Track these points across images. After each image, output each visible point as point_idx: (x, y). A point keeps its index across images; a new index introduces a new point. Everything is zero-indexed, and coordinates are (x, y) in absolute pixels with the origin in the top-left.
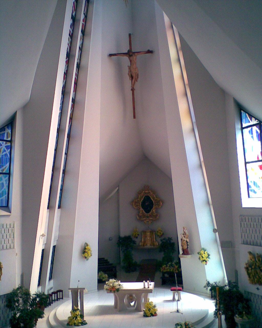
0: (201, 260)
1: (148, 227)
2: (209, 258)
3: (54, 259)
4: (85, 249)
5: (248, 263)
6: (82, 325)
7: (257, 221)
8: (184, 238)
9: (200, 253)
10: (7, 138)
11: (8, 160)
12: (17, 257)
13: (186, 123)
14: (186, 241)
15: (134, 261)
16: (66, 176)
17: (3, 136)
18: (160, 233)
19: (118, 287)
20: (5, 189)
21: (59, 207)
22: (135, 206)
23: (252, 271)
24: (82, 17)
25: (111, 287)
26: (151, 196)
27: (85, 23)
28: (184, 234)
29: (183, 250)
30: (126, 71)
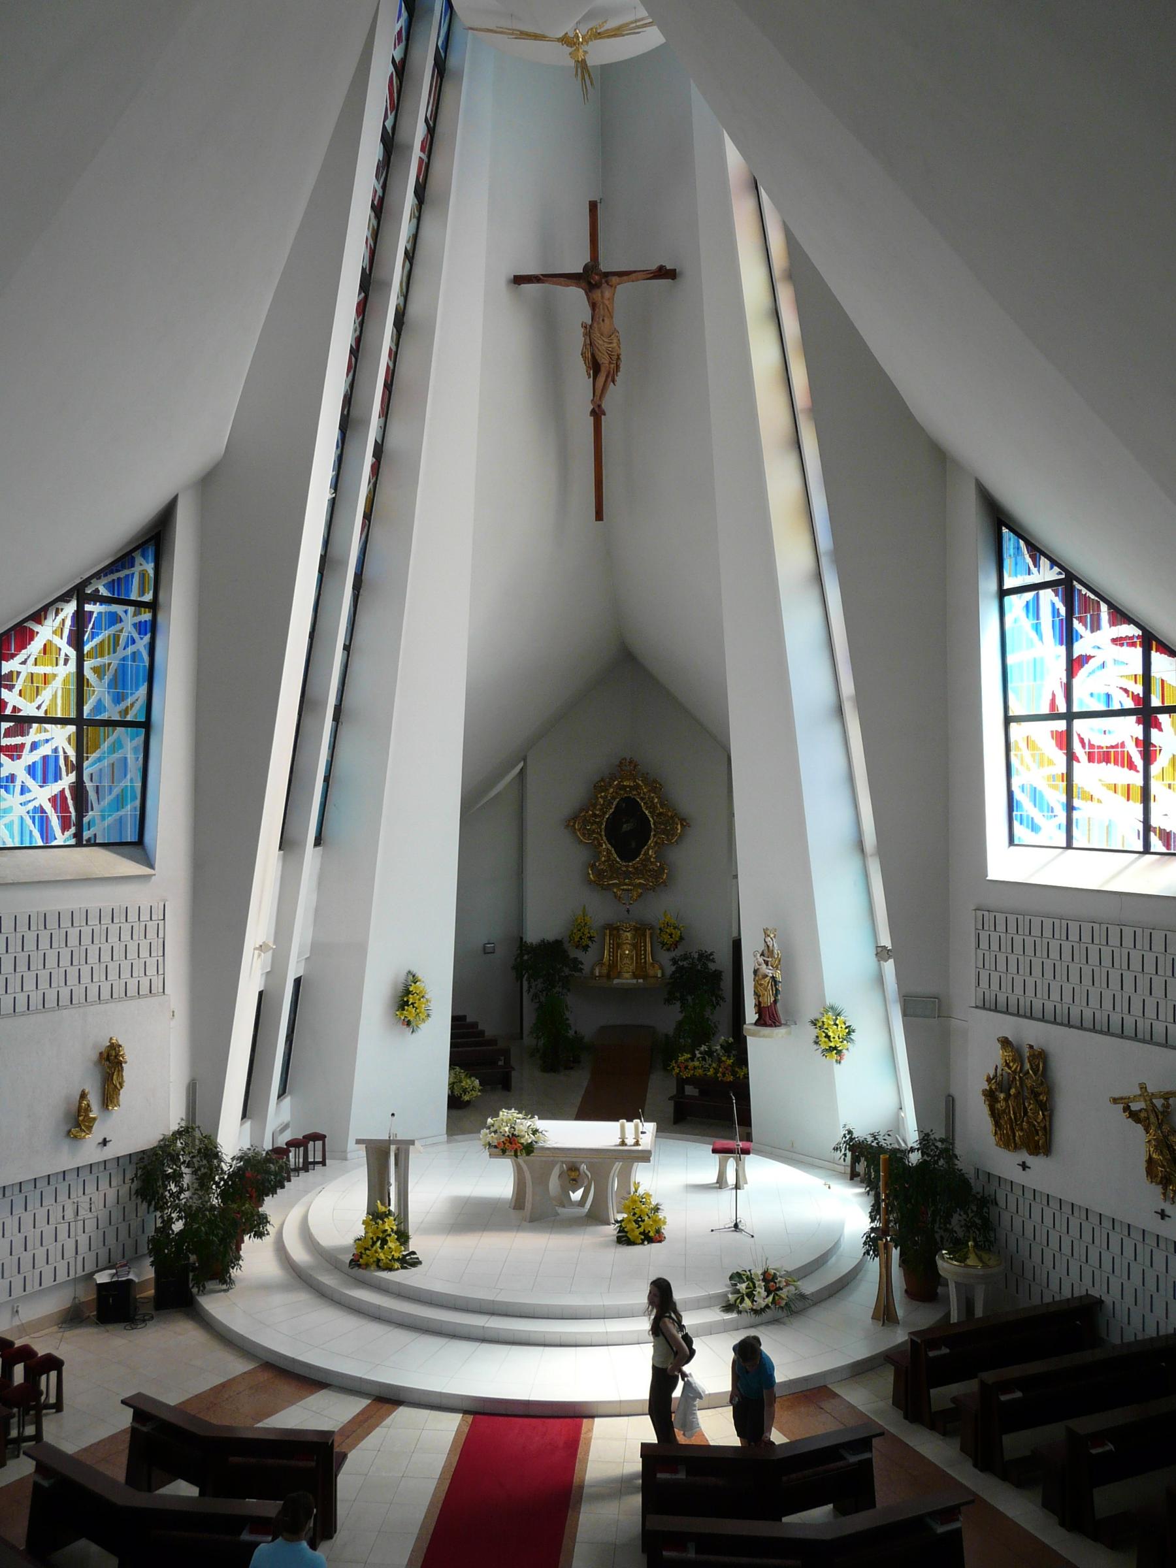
0: (823, 1047)
1: (628, 911)
2: (851, 1041)
3: (298, 1027)
4: (408, 992)
5: (995, 1076)
6: (403, 1268)
7: (1036, 931)
8: (764, 966)
9: (820, 1024)
10: (142, 592)
11: (143, 674)
12: (173, 1023)
13: (792, 555)
14: (773, 978)
15: (571, 1033)
16: (344, 730)
17: (128, 591)
18: (671, 935)
19: (528, 1138)
20: (131, 780)
21: (318, 842)
22: (584, 835)
23: (1008, 1106)
24: (421, 131)
25: (503, 1139)
26: (642, 799)
27: (429, 157)
28: (766, 952)
29: (760, 1009)
30: (577, 340)
